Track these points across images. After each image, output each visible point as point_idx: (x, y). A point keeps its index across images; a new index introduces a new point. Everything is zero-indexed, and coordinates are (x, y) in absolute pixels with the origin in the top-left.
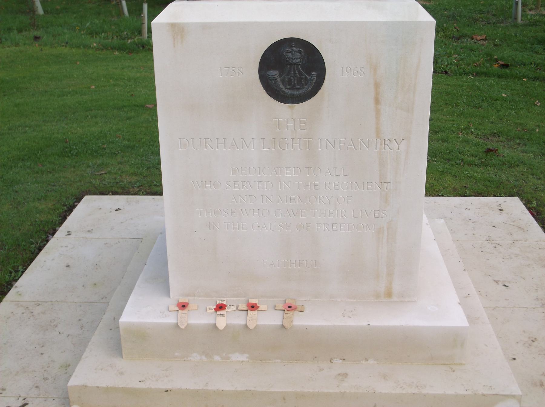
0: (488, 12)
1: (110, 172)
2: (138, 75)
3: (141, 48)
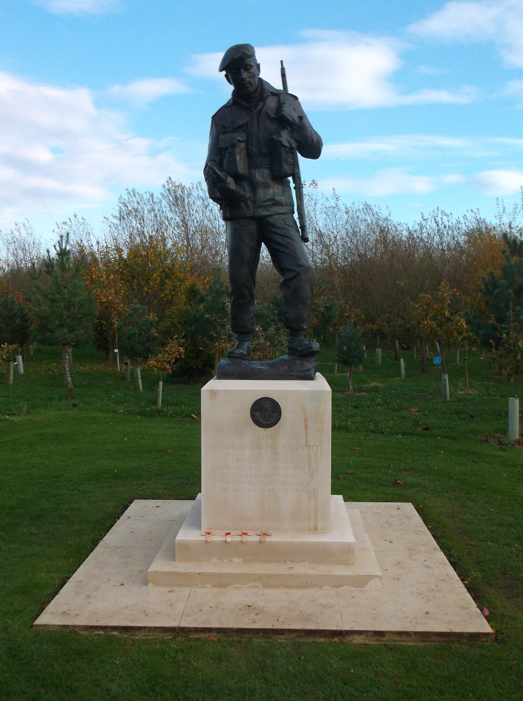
0: (426, 391)
1: (149, 488)
2: (158, 432)
3: (157, 414)
